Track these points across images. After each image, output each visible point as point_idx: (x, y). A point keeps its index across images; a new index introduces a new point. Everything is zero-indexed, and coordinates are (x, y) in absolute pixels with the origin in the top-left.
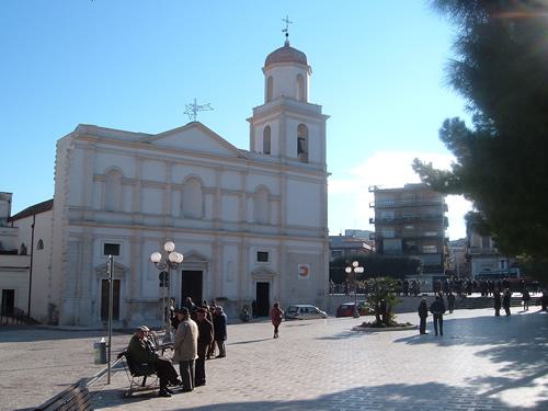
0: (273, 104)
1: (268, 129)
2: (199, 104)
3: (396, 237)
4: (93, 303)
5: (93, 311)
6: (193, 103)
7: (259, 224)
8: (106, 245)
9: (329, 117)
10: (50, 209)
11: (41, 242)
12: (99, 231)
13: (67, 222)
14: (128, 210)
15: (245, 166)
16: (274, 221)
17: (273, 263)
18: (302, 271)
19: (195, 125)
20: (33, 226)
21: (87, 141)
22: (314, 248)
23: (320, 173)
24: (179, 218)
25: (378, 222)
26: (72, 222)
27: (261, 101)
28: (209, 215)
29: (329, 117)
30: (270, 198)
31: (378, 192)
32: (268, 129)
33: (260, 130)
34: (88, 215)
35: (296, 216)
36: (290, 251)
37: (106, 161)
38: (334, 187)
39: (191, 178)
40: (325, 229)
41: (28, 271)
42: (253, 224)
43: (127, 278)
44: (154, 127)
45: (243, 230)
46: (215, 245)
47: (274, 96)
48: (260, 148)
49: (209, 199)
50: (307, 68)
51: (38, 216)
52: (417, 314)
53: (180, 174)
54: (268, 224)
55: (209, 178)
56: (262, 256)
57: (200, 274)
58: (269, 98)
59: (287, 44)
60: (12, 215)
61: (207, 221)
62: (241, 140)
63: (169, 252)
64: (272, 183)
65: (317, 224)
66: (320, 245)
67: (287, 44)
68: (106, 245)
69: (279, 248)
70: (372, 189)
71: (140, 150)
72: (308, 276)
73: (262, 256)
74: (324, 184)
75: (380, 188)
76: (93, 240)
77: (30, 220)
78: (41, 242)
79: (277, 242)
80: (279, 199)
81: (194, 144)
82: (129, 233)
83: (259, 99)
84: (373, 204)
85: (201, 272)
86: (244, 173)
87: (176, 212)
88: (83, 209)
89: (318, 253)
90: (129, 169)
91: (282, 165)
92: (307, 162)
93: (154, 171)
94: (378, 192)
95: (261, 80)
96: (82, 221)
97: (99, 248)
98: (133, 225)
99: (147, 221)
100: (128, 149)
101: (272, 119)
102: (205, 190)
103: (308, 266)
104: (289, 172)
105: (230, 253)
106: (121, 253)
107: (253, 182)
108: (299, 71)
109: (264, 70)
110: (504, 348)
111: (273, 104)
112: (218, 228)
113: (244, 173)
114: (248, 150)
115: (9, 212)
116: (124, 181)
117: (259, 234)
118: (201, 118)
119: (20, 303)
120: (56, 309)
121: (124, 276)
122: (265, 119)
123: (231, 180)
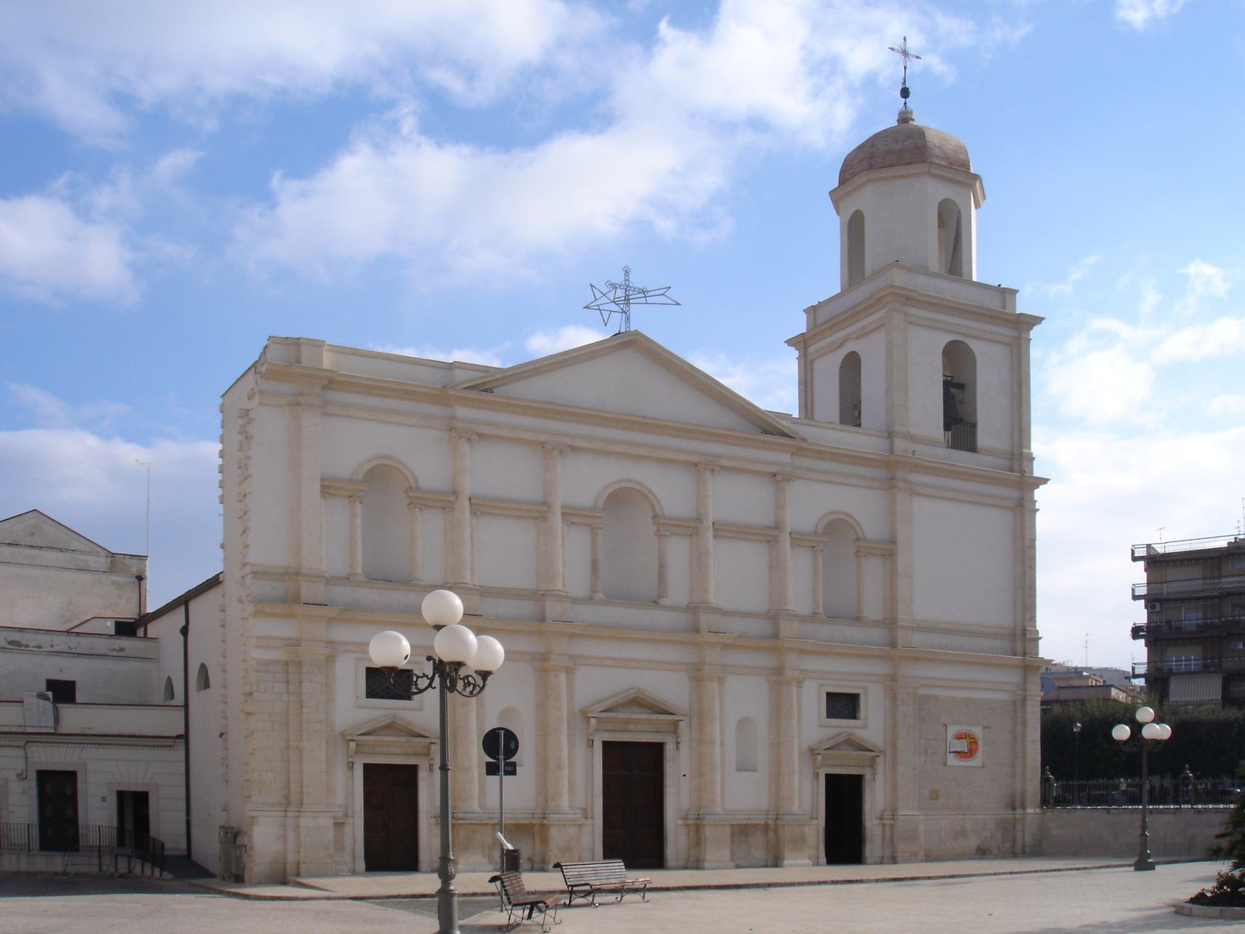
0: (861, 293)
1: (852, 365)
2: (637, 281)
3: (1206, 670)
4: (339, 825)
5: (339, 846)
6: (619, 279)
8: (829, 694)
9: (1039, 320)
13: (250, 608)
15: (786, 458)
17: (871, 724)
18: (962, 746)
19: (629, 343)
20: (185, 631)
22: (998, 684)
23: (1017, 482)
24: (589, 600)
25: (1154, 634)
28: (678, 592)
29: (1039, 320)
30: (863, 548)
31: (1155, 562)
32: (852, 365)
36: (922, 692)
37: (353, 442)
38: (1052, 511)
40: (1023, 635)
41: (182, 742)
42: (813, 618)
43: (684, 738)
45: (771, 638)
46: (697, 675)
47: (869, 266)
49: (677, 550)
50: (958, 171)
53: (584, 481)
55: (671, 491)
56: (843, 705)
57: (655, 752)
59: (904, 118)
62: (772, 385)
64: (861, 505)
65: (999, 616)
66: (1014, 677)
67: (904, 118)
68: (829, 694)
69: (892, 685)
70: (1142, 552)
72: (977, 761)
73: (843, 705)
74: (1023, 510)
75: (1160, 550)
76: (330, 659)
77: (178, 617)
78: (203, 669)
79: (881, 668)
80: (888, 550)
83: (825, 279)
84: (1143, 591)
86: (777, 478)
88: (293, 574)
90: (421, 454)
91: (891, 471)
92: (972, 448)
94: (1155, 562)
97: (350, 683)
101: (865, 333)
102: (664, 526)
103: (977, 731)
105: (740, 699)
107: (809, 504)
108: (938, 191)
109: (837, 197)
110: (1223, 803)
111: (861, 293)
112: (695, 624)
113: (777, 478)
115: (141, 603)
116: (420, 499)
118: (647, 321)
119: (166, 824)
120: (240, 841)
122: (839, 335)
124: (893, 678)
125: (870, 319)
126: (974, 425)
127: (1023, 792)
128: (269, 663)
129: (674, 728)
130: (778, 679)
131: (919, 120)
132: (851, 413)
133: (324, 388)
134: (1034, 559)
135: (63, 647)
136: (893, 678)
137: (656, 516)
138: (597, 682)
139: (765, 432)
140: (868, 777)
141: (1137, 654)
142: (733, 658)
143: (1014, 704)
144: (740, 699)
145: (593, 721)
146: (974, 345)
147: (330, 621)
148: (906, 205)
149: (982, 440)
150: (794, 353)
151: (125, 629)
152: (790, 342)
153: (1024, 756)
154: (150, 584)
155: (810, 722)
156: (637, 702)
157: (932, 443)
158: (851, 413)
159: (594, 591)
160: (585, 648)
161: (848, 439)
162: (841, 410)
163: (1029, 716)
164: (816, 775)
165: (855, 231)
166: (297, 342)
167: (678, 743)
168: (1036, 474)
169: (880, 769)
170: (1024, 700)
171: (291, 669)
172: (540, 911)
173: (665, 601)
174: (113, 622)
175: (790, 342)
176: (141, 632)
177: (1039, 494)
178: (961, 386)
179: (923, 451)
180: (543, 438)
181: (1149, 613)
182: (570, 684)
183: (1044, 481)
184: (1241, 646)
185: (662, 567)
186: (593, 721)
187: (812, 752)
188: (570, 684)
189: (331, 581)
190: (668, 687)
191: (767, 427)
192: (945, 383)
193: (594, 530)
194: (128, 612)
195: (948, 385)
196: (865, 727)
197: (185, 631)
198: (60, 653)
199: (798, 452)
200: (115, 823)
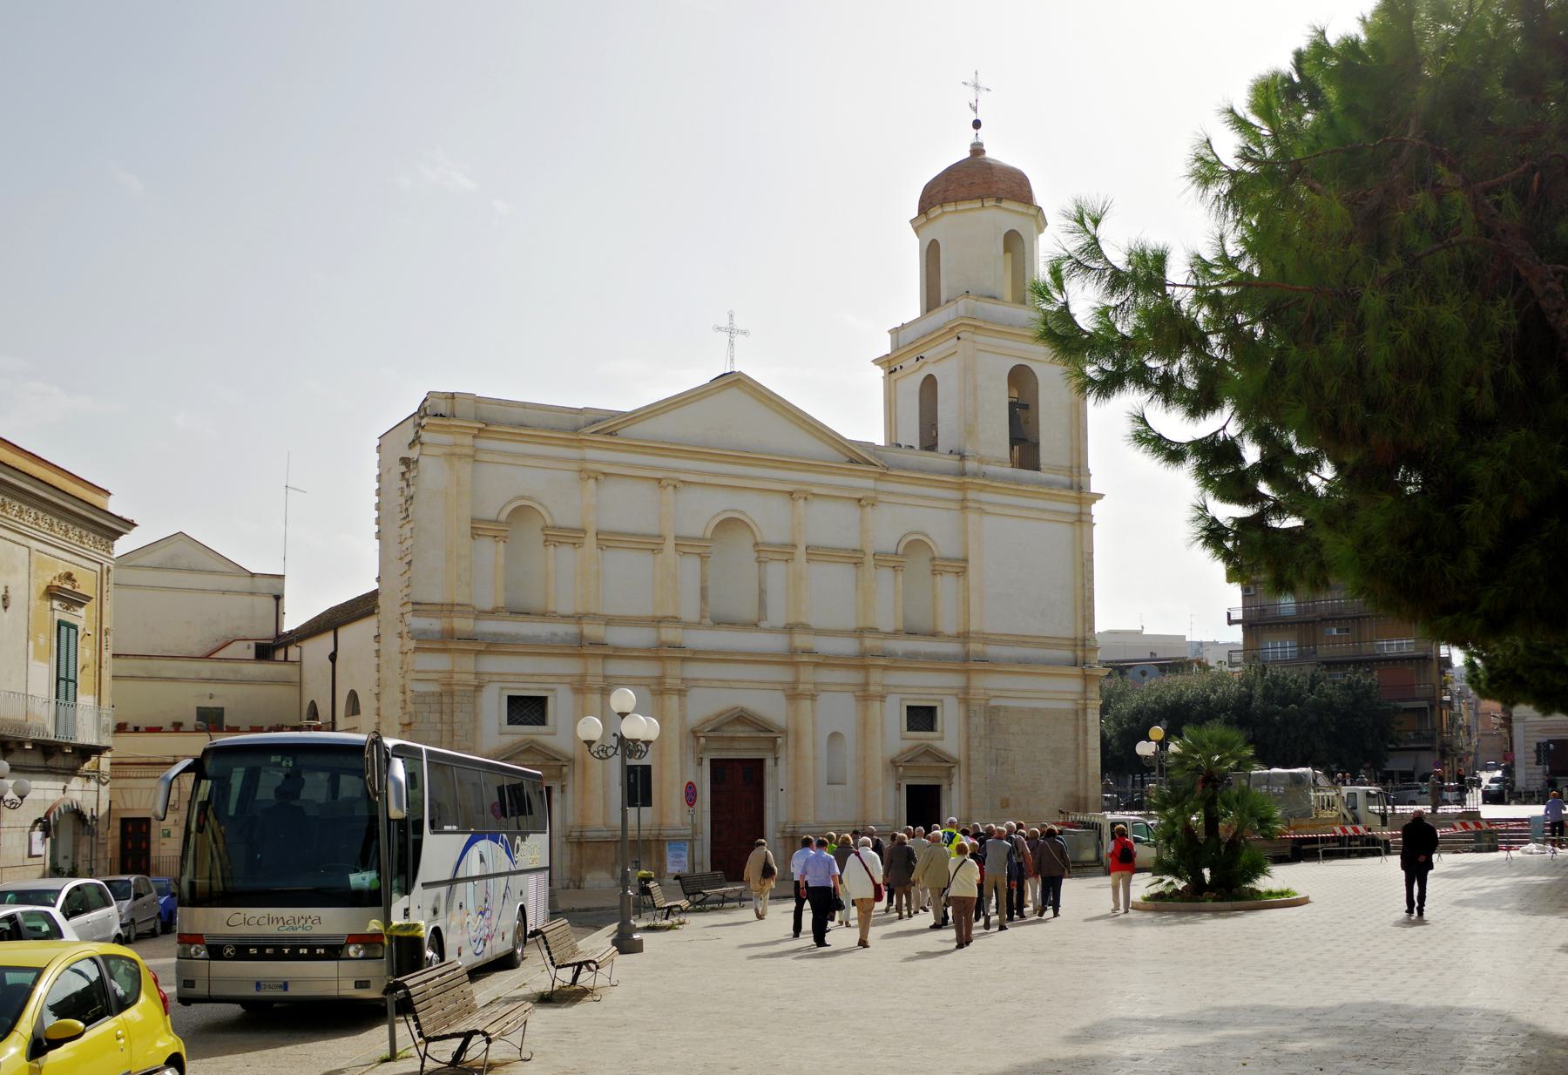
1: (930, 384)
6: (725, 323)
7: (911, 633)
8: (510, 698)
10: (370, 613)
11: (353, 697)
12: (491, 664)
14: (566, 608)
15: (870, 483)
16: (948, 625)
17: (949, 736)
20: (333, 657)
21: (446, 430)
26: (424, 643)
27: (910, 307)
28: (777, 615)
30: (938, 566)
32: (930, 384)
33: (911, 385)
34: (463, 624)
35: (1002, 601)
36: (993, 703)
37: (507, 479)
39: (729, 524)
44: (627, 388)
46: (794, 694)
48: (911, 433)
51: (346, 633)
52: (1396, 860)
53: (698, 511)
54: (934, 634)
55: (769, 518)
56: (922, 717)
58: (932, 299)
59: (977, 150)
60: (290, 624)
61: (771, 630)
62: (859, 412)
63: (623, 715)
66: (1075, 685)
67: (977, 150)
68: (510, 698)
69: (965, 698)
71: (590, 453)
73: (922, 717)
74: (1083, 520)
76: (479, 688)
77: (324, 642)
78: (353, 697)
79: (956, 680)
80: (960, 567)
81: (735, 430)
82: (570, 667)
85: (761, 762)
87: (690, 611)
89: (1068, 705)
93: (626, 506)
95: (910, 249)
96: (448, 641)
97: (493, 706)
98: (581, 647)
99: (992, 650)
100: (1041, 504)
102: (764, 552)
104: (984, 496)
106: (939, 725)
107: (887, 527)
109: (917, 225)
111: (942, 316)
114: (880, 440)
117: (912, 662)
121: (949, 776)
123: (830, 523)
124: (966, 689)
125: (941, 348)
126: (1037, 445)
127: (1086, 799)
128: (424, 695)
129: (774, 746)
130: (865, 696)
131: (993, 153)
132: (929, 442)
133: (475, 436)
134: (1092, 572)
135: (206, 674)
136: (966, 689)
137: (756, 544)
138: (705, 705)
139: (851, 461)
140: (945, 787)
141: (1236, 635)
142: (825, 675)
143: (1076, 711)
144: (834, 710)
145: (702, 740)
146: (1033, 366)
147: (478, 653)
148: (983, 222)
149: (1044, 458)
150: (879, 373)
151: (264, 652)
152: (877, 362)
153: (1086, 765)
154: (288, 603)
155: (893, 735)
156: (742, 718)
157: (1000, 462)
158: (929, 442)
159: (703, 617)
160: (694, 670)
161: (928, 458)
162: (921, 423)
163: (1090, 724)
164: (898, 787)
165: (932, 254)
166: (453, 396)
167: (776, 759)
168: (1093, 490)
169: (955, 780)
170: (1085, 709)
171: (445, 699)
172: (590, 969)
173: (763, 624)
174: (252, 644)
175: (877, 362)
176: (280, 655)
177: (1097, 509)
178: (1026, 407)
179: (992, 469)
180: (659, 475)
181: (1244, 597)
182: (682, 706)
183: (1101, 496)
184: (1335, 632)
185: (762, 593)
186: (702, 740)
187: (894, 763)
188: (682, 706)
189: (480, 614)
190: (769, 706)
191: (856, 456)
192: (1012, 406)
193: (703, 558)
194: (266, 632)
195: (1013, 406)
196: (941, 739)
197: (333, 657)
198: (208, 680)
199: (882, 476)
200: (179, 853)
